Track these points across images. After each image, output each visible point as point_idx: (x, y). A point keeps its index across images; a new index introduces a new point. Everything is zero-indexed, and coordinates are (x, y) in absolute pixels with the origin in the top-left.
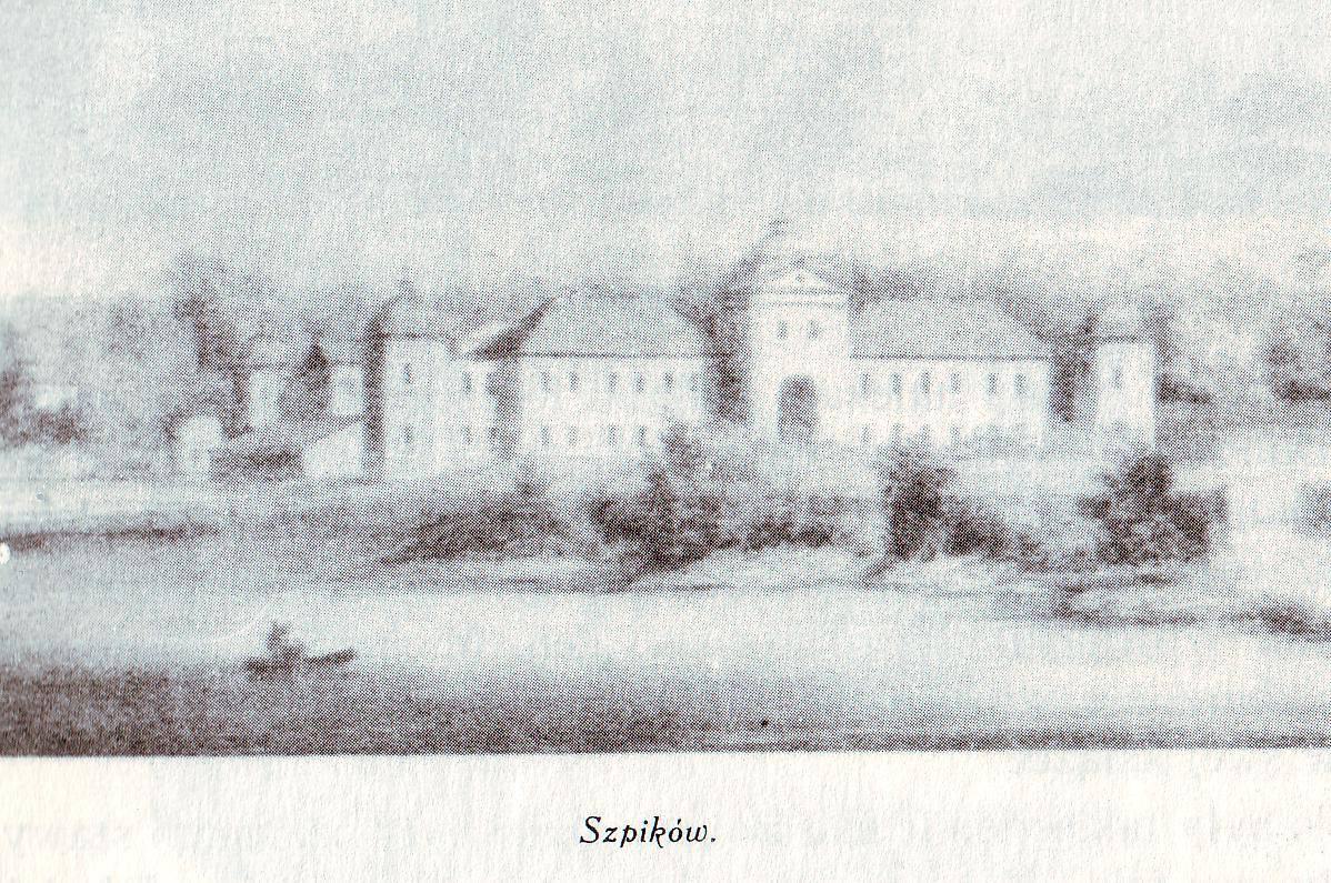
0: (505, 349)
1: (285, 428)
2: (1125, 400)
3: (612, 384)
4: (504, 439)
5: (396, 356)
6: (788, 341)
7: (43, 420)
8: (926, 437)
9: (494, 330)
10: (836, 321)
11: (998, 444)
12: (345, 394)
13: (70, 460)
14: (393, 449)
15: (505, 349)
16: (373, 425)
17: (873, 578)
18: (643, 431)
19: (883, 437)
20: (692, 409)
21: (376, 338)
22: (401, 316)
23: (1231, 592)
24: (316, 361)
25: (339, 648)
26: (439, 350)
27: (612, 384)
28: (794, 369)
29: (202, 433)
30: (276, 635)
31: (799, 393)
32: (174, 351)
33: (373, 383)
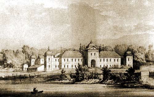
0: (60, 57)
1: (37, 67)
2: (130, 62)
3: (91, 55)
4: (60, 66)
5: (48, 57)
6: (93, 55)
7: (8, 65)
8: (76, 6)
9: (59, 54)
10: (97, 54)
11: (116, 67)
12: (42, 62)
13: (11, 70)
14: (47, 68)
15: (60, 57)
16: (45, 65)
17: (101, 83)
18: (75, 66)
19: (102, 66)
20: (81, 63)
21: (45, 56)
22: (49, 53)
23: (141, 84)
24: (39, 58)
25: (41, 90)
26: (53, 57)
27: (91, 55)
28: (93, 59)
29: (26, 66)
30: (34, 89)
31: (93, 62)
32: (22, 56)
33: (45, 60)
